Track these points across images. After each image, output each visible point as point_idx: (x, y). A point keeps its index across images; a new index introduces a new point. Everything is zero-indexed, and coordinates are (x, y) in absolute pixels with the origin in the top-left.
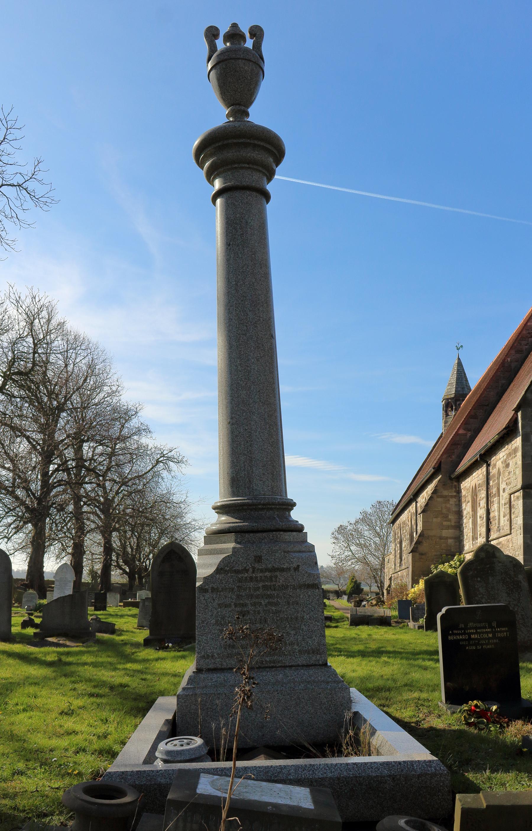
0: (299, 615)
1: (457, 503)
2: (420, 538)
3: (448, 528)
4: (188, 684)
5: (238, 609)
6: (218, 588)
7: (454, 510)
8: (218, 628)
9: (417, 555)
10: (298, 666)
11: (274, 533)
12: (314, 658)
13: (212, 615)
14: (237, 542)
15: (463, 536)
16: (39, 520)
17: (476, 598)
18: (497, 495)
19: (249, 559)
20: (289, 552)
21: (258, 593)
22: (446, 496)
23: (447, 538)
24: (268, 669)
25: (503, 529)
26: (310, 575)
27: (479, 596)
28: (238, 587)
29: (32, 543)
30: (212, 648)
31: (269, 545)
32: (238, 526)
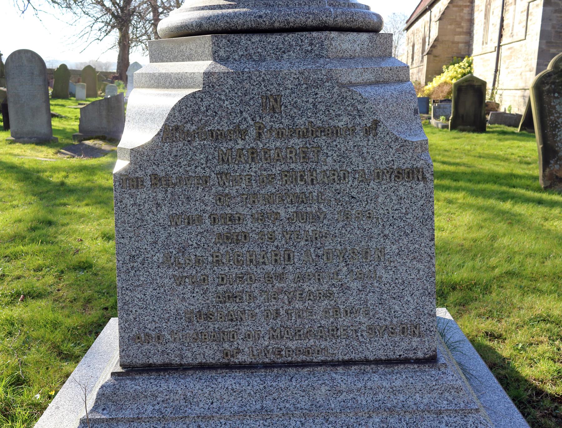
0: (373, 244)
1: (470, 12)
2: (436, 43)
3: (460, 34)
4: (95, 408)
5: (220, 228)
6: (167, 178)
7: (466, 18)
8: (170, 272)
9: (432, 57)
10: (367, 362)
11: (315, 34)
12: (404, 345)
13: (156, 243)
14: (217, 58)
15: (473, 41)
16: (123, 25)
17: (551, 117)
18: (513, 3)
19: (248, 104)
20: (351, 84)
21: (270, 188)
22: (460, 6)
23: (458, 43)
24: (292, 371)
25: (517, 35)
26: (404, 145)
27: (555, 115)
28: (220, 173)
29: (119, 43)
30: (156, 319)
31: (302, 68)
32: (223, 16)
